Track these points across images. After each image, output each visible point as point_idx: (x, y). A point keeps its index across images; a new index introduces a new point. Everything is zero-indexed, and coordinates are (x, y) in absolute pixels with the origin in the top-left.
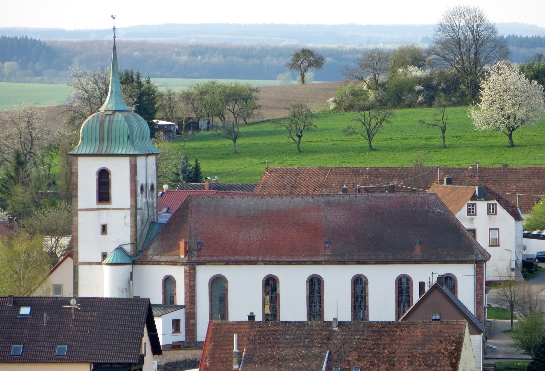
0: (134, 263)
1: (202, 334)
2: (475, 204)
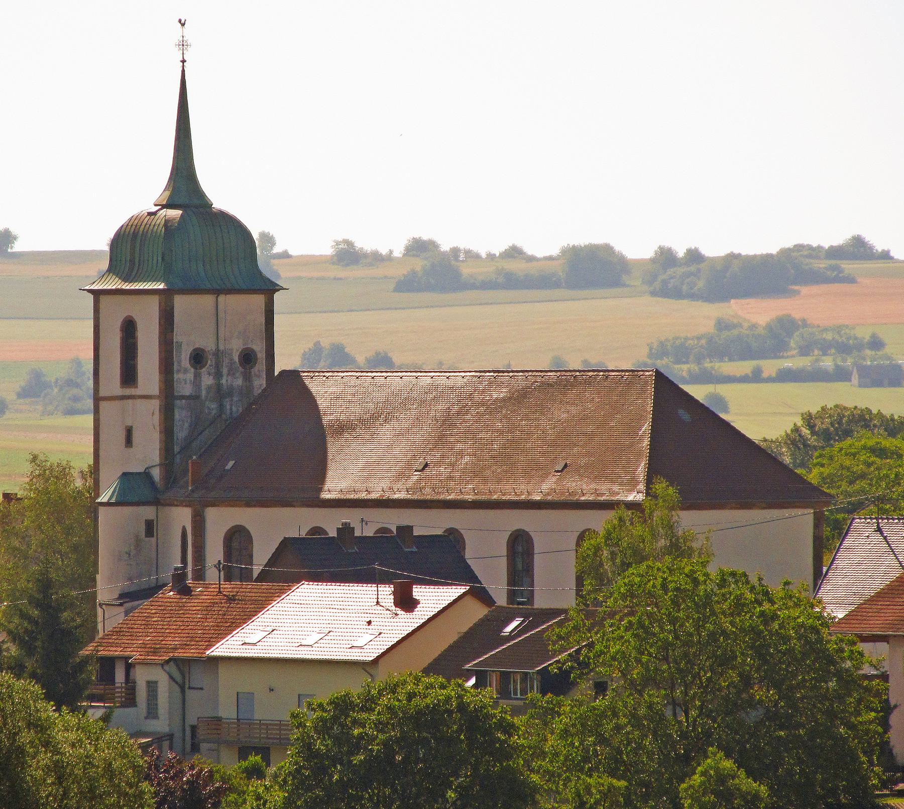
0: (156, 502)
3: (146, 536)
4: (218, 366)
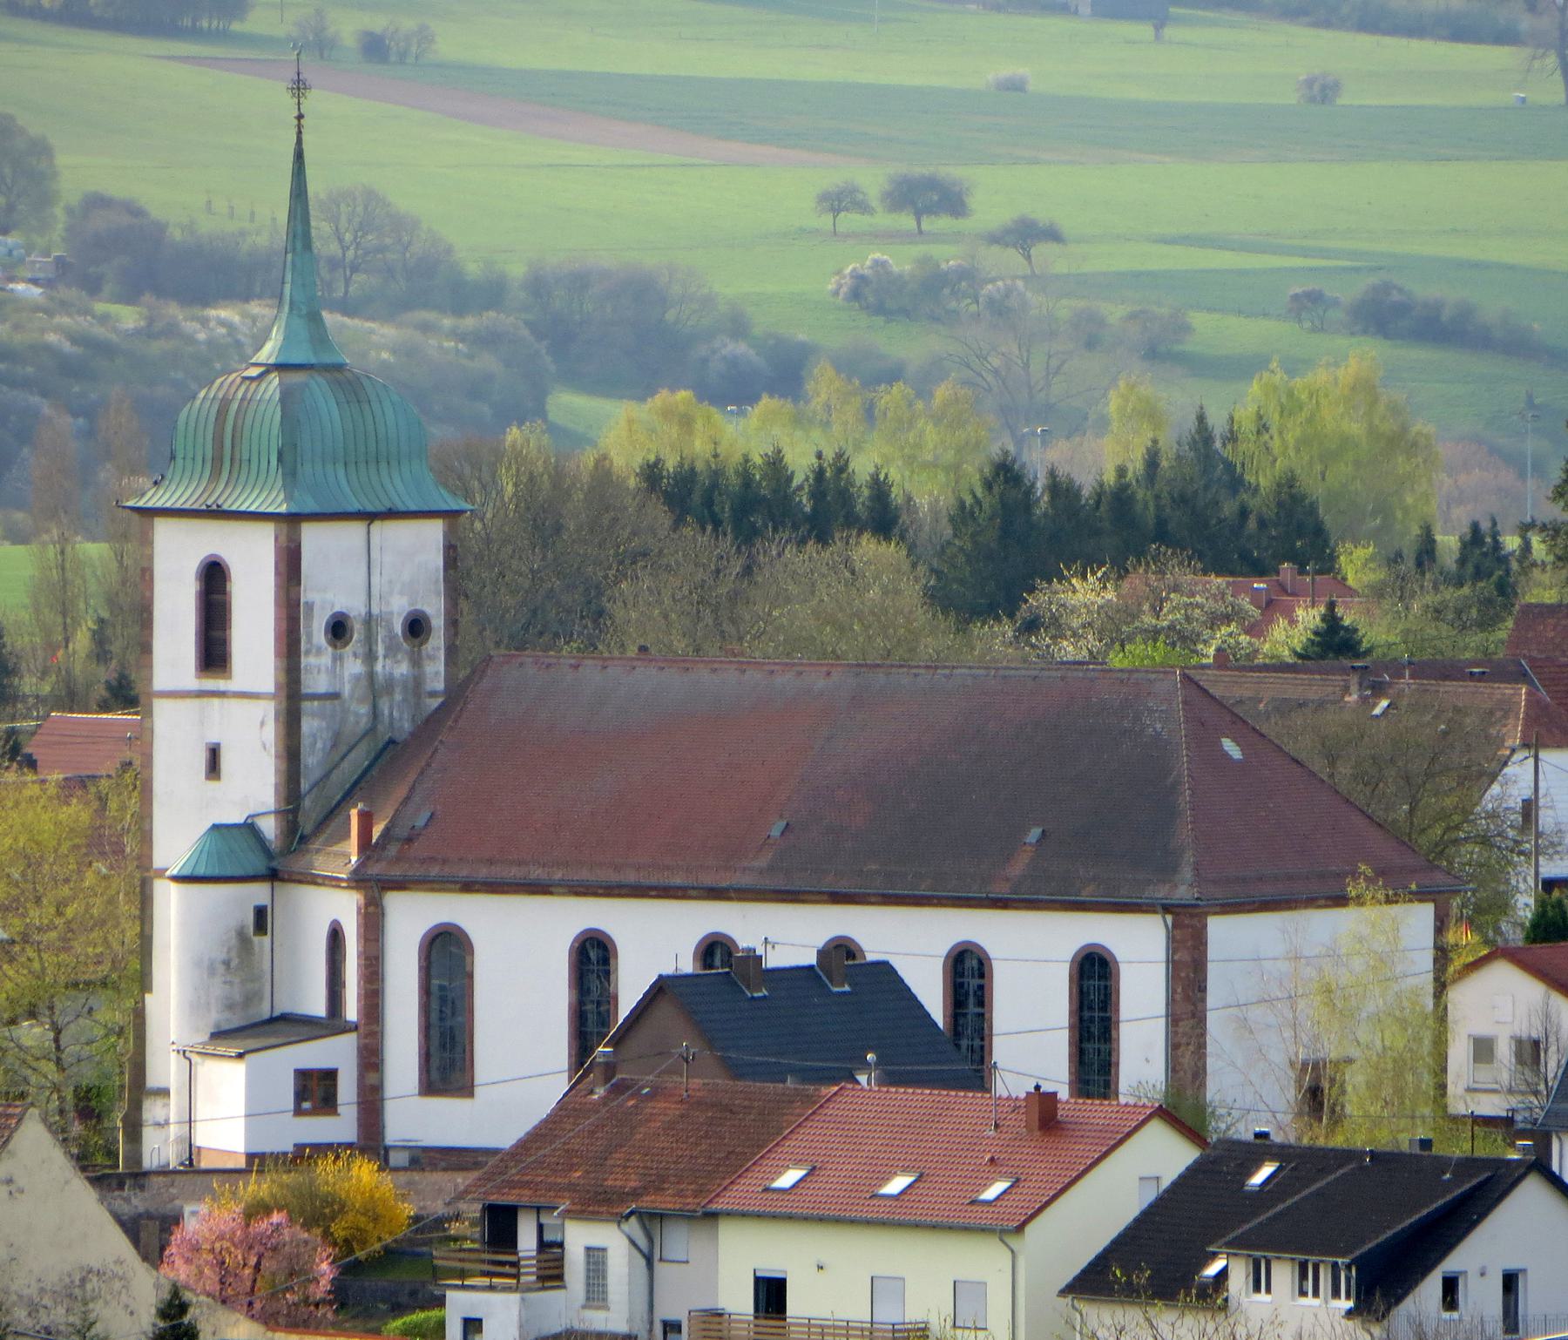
0: (273, 876)
3: (255, 934)
4: (369, 640)
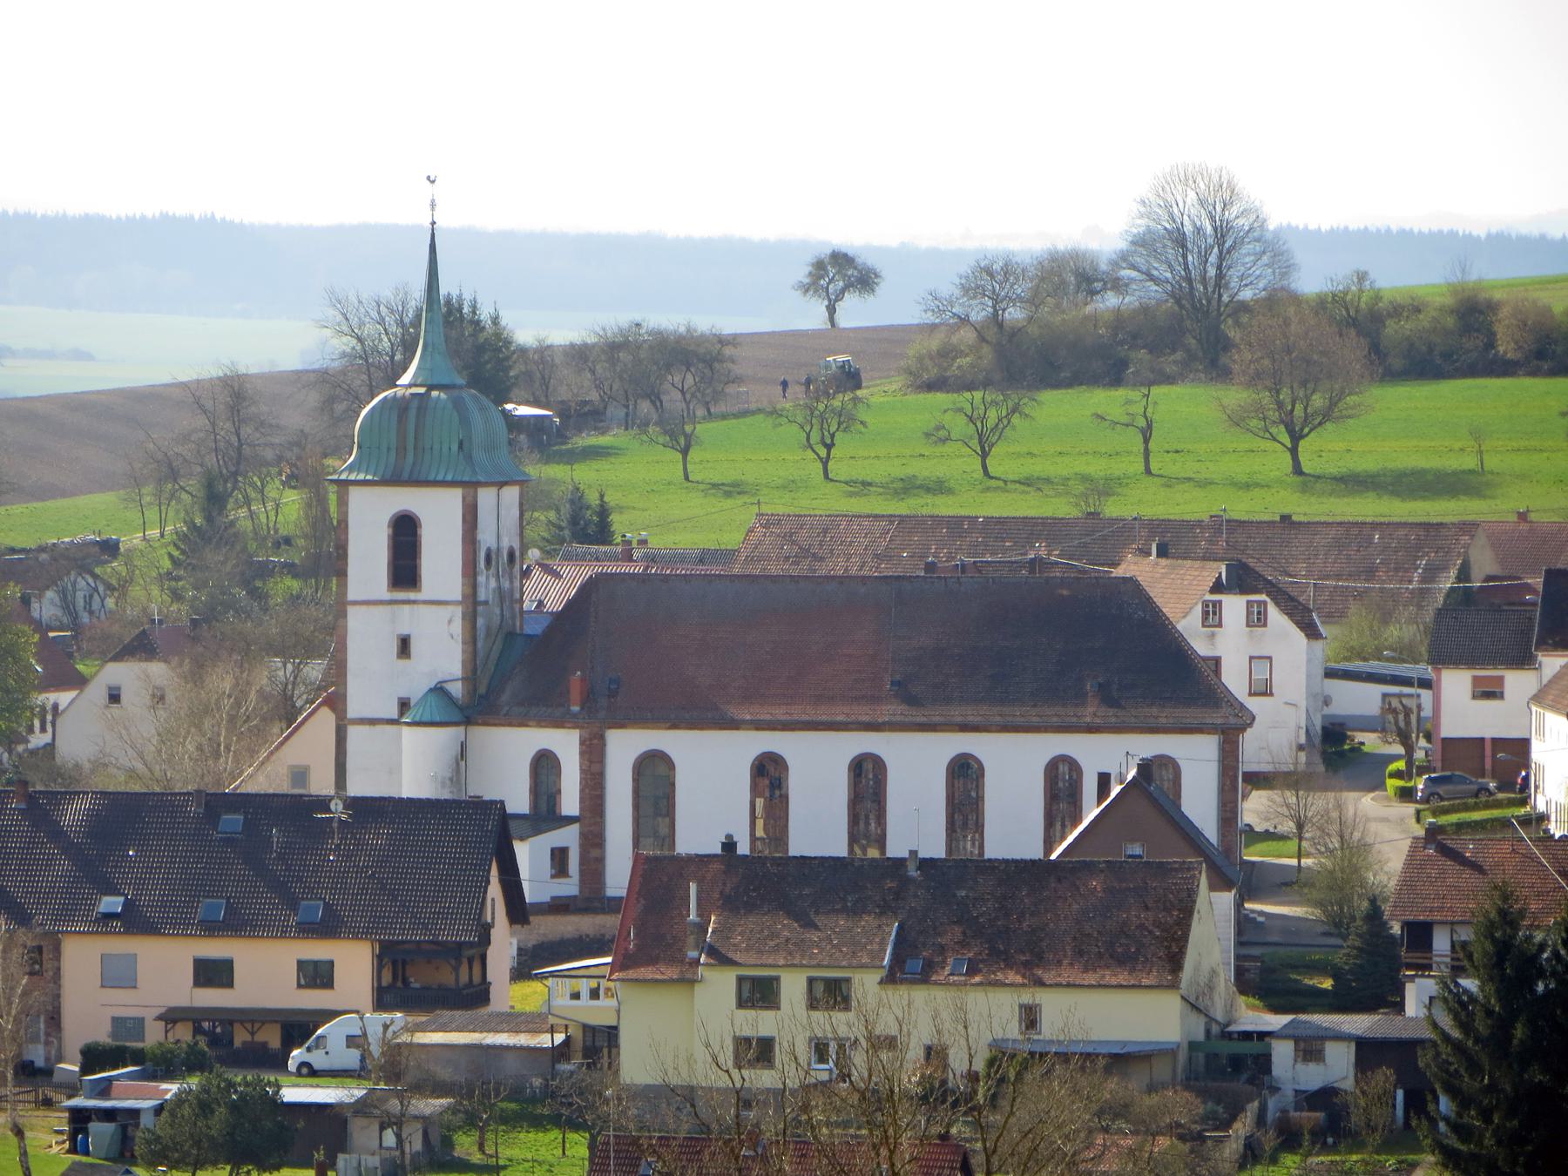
0: (468, 721)
1: (618, 876)
2: (1220, 602)
